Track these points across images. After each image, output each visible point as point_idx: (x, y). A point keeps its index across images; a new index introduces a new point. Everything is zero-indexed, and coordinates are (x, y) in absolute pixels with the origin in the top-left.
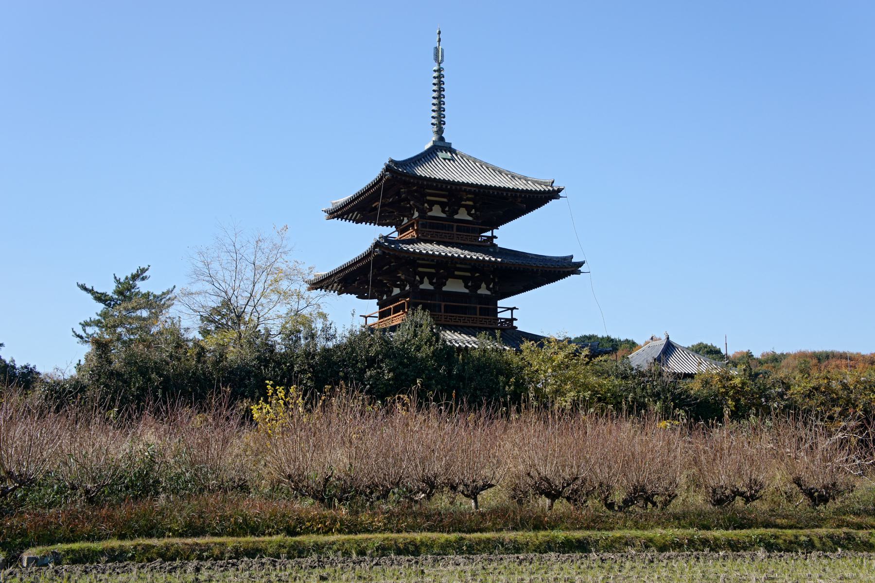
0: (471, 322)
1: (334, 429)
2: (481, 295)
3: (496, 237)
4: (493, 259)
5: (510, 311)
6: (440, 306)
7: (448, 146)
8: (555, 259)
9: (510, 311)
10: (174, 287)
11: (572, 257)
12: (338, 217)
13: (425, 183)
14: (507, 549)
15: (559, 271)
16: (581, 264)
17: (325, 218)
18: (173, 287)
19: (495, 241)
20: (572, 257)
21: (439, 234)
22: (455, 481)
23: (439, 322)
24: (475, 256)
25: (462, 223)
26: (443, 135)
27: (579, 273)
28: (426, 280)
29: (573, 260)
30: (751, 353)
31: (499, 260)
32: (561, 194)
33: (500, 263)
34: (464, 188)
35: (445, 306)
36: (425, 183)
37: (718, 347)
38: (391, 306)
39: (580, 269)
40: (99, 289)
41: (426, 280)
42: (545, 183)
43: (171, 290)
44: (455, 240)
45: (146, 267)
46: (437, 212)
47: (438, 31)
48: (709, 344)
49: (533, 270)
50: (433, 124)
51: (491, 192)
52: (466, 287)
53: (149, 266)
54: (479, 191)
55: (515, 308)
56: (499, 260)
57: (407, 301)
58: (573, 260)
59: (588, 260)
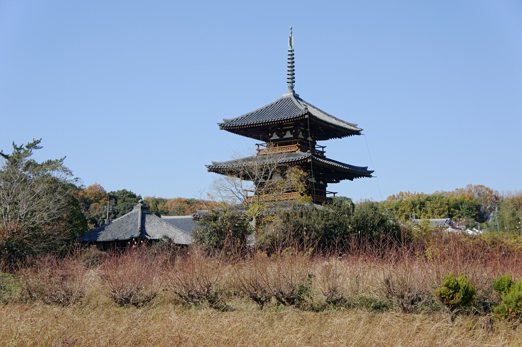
1: (493, 246)
4: (342, 167)
10: (65, 157)
11: (367, 167)
14: (313, 309)
16: (372, 172)
17: (219, 129)
18: (64, 157)
20: (367, 167)
22: (420, 267)
27: (370, 176)
29: (368, 169)
30: (141, 197)
31: (348, 168)
33: (348, 169)
37: (134, 193)
40: (64, 161)
43: (63, 159)
45: (39, 140)
47: (291, 27)
48: (129, 191)
50: (288, 82)
53: (41, 139)
58: (368, 169)
59: (375, 170)
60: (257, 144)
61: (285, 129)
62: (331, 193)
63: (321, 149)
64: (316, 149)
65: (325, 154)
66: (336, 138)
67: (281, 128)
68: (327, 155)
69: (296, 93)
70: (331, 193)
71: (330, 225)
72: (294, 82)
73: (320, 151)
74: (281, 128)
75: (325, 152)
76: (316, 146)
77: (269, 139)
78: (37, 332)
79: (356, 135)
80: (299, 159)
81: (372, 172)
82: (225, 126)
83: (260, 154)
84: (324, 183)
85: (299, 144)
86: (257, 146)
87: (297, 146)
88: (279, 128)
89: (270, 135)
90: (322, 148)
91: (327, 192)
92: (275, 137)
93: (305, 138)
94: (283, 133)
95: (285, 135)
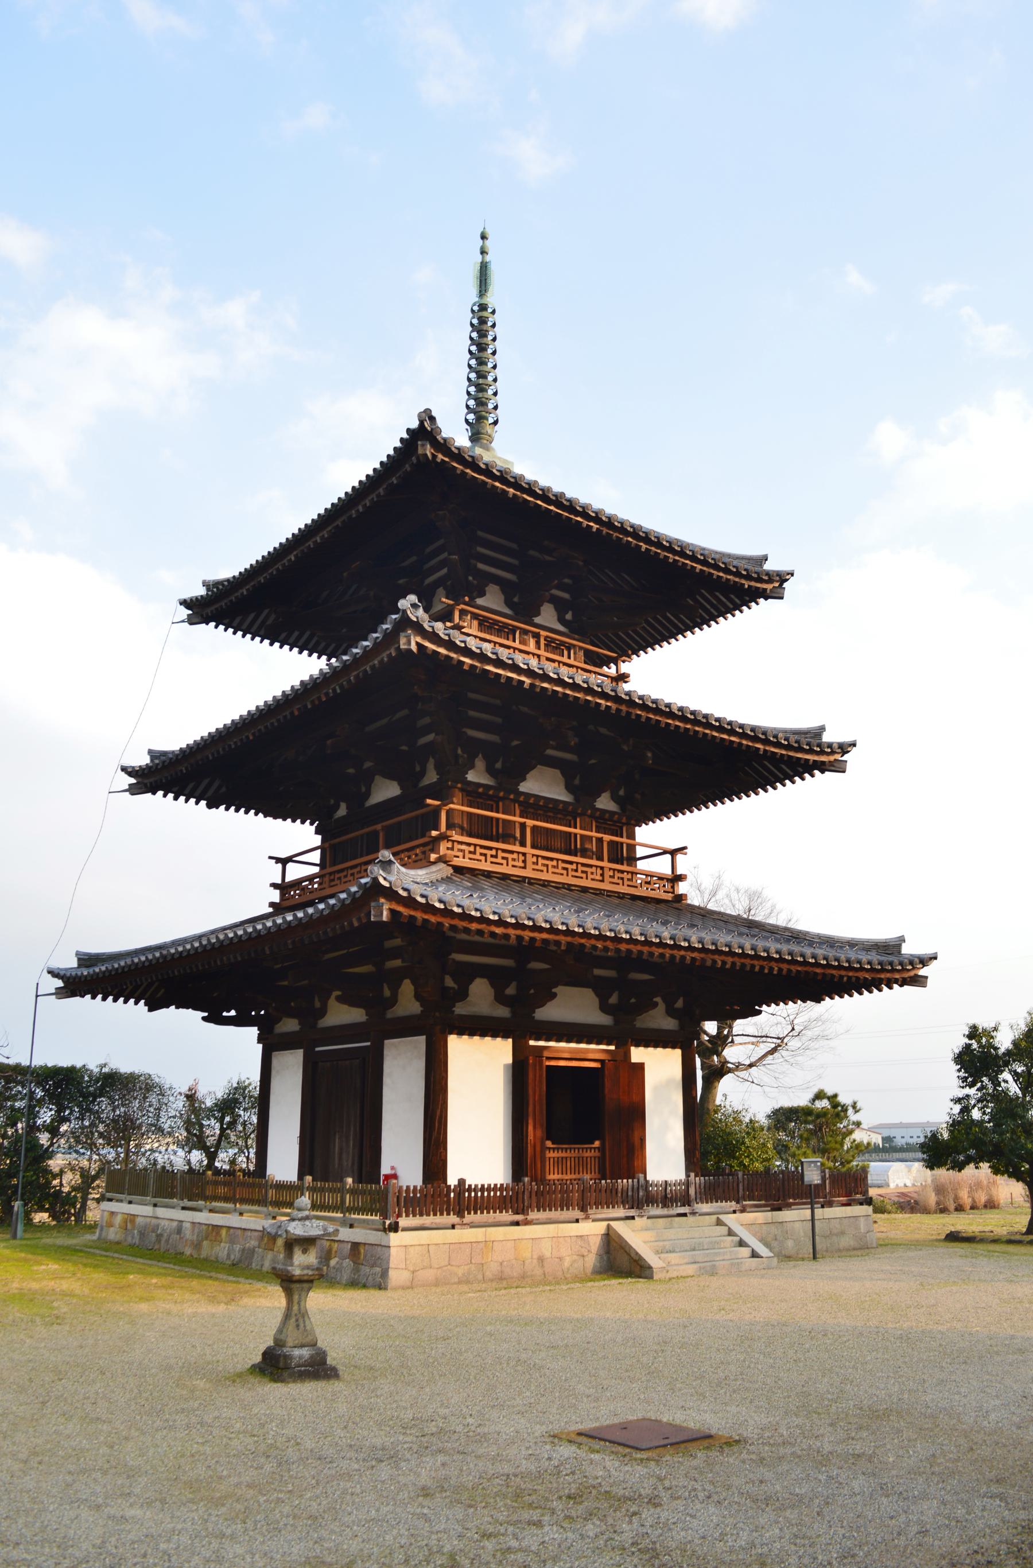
9: (668, 857)
19: (682, 888)
28: (480, 763)
29: (906, 949)
41: (480, 763)
55: (682, 850)
58: (906, 949)
60: (278, 860)
63: (662, 866)
65: (682, 888)
86: (280, 865)
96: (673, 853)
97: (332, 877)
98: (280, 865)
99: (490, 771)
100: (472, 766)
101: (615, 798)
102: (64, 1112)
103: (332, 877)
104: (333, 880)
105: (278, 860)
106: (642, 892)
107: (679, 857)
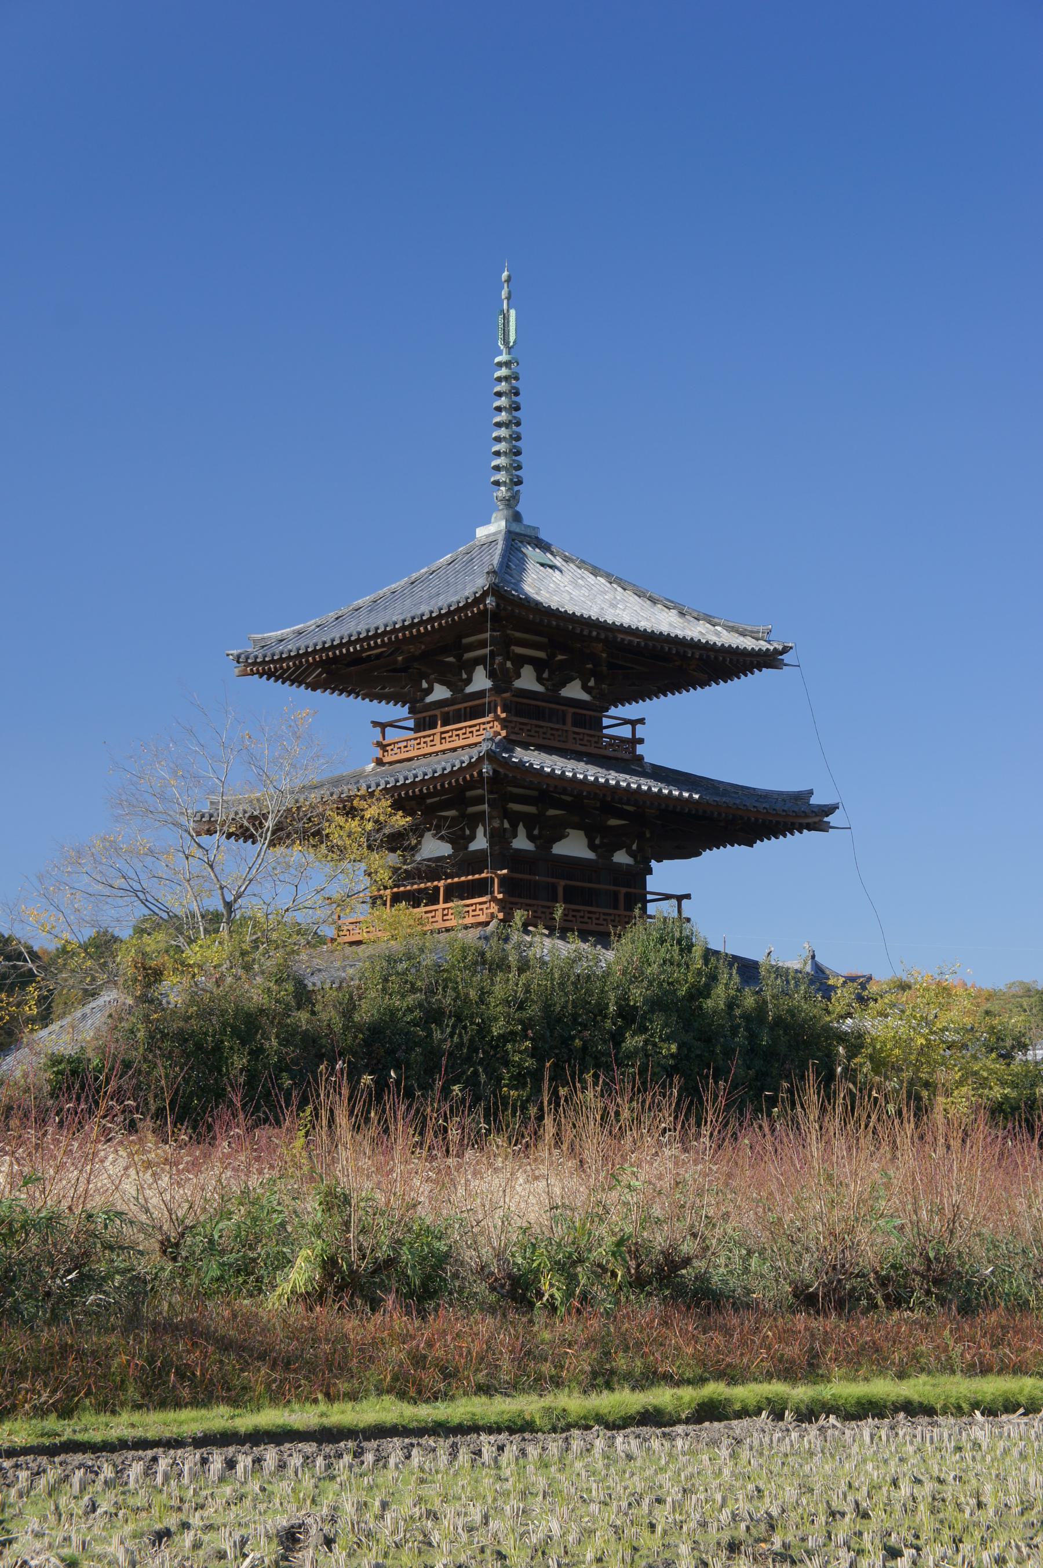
0: (595, 921)
2: (519, 851)
3: (641, 741)
5: (674, 902)
6: (554, 888)
7: (533, 534)
8: (775, 796)
9: (674, 902)
11: (810, 793)
12: (270, 675)
13: (554, 623)
15: (771, 821)
16: (830, 810)
19: (640, 750)
20: (810, 793)
21: (541, 730)
23: (584, 927)
24: (614, 778)
25: (582, 708)
26: (518, 508)
28: (521, 831)
29: (814, 800)
31: (696, 796)
32: (786, 658)
33: (697, 802)
34: (620, 636)
35: (565, 888)
36: (554, 623)
38: (441, 884)
39: (826, 819)
41: (521, 831)
42: (752, 632)
44: (569, 746)
46: (527, 681)
49: (749, 819)
51: (667, 649)
52: (592, 847)
54: (646, 644)
55: (688, 896)
56: (696, 796)
57: (498, 876)
58: (814, 800)
60: (375, 724)
61: (469, 660)
62: (667, 897)
63: (625, 732)
64: (605, 731)
65: (640, 750)
66: (695, 689)
67: (459, 658)
68: (650, 753)
69: (527, 520)
70: (667, 897)
71: (410, 1010)
72: (519, 482)
73: (623, 740)
74: (459, 658)
75: (641, 741)
76: (606, 722)
77: (423, 699)
78: (946, 1360)
79: (767, 668)
80: (455, 769)
81: (830, 810)
82: (250, 661)
83: (386, 760)
84: (635, 860)
85: (502, 712)
86: (379, 729)
87: (497, 718)
88: (451, 659)
89: (425, 685)
90: (629, 727)
91: (649, 897)
92: (440, 693)
93: (547, 689)
94: (465, 676)
95: (469, 681)
96: (680, 898)
97: (446, 912)
98: (379, 729)
99: (530, 837)
100: (515, 836)
101: (630, 853)
102: (391, 1077)
103: (446, 912)
104: (447, 915)
105: (375, 724)
106: (609, 752)
107: (684, 902)
